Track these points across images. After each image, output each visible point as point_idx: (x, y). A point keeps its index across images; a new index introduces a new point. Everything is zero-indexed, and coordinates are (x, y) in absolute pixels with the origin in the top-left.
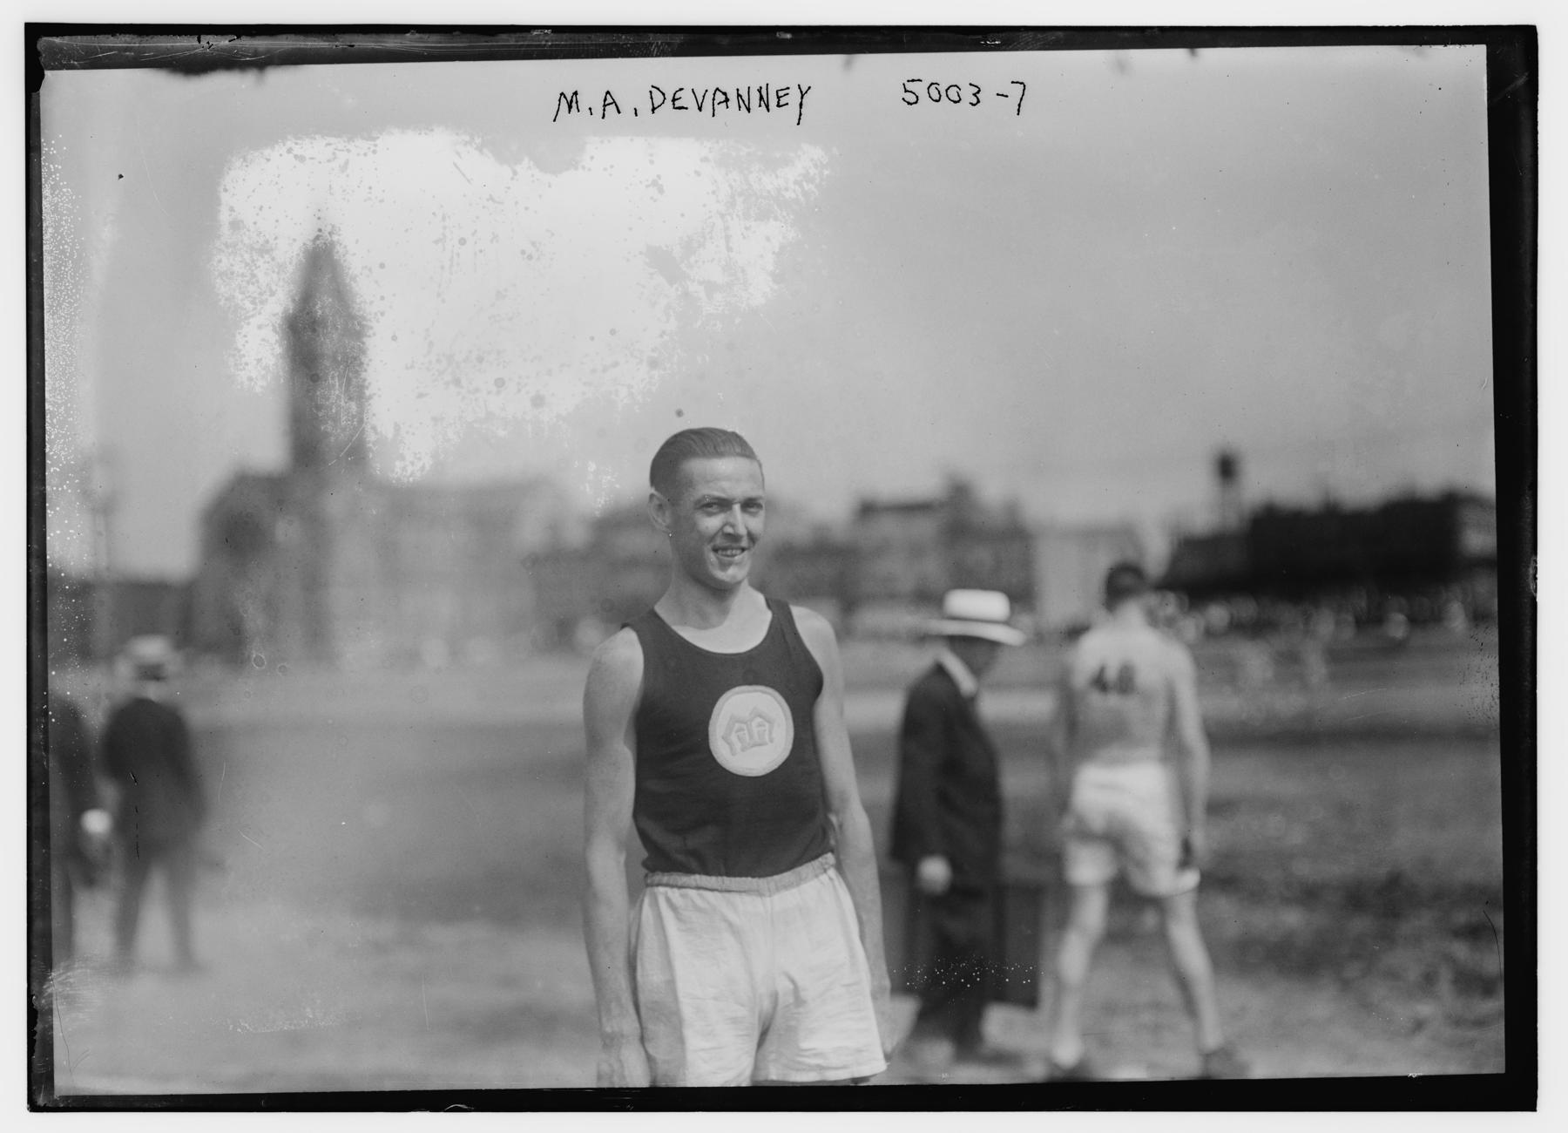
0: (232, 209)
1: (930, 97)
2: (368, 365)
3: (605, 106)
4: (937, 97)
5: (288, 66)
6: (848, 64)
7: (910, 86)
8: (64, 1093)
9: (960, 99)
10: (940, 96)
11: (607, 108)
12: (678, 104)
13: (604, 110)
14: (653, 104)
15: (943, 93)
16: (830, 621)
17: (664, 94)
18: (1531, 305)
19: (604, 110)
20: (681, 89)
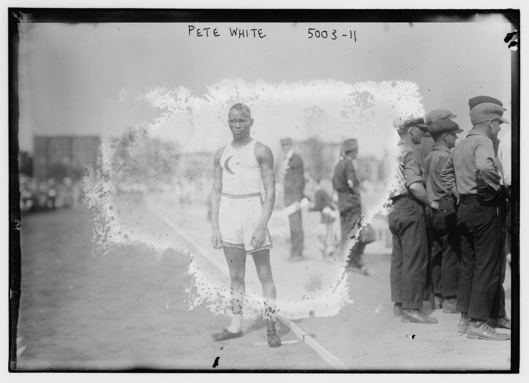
0: (241, 96)
1: (316, 36)
2: (92, 193)
3: (190, 31)
4: (318, 36)
5: (79, 23)
6: (294, 26)
7: (311, 31)
8: (18, 24)
9: (336, 37)
10: (320, 35)
11: (241, 35)
12: (262, 35)
13: (190, 32)
14: (240, 33)
15: (320, 34)
16: (18, 35)
17: (327, 35)
18: (513, 151)
19: (190, 32)
20: (261, 30)
